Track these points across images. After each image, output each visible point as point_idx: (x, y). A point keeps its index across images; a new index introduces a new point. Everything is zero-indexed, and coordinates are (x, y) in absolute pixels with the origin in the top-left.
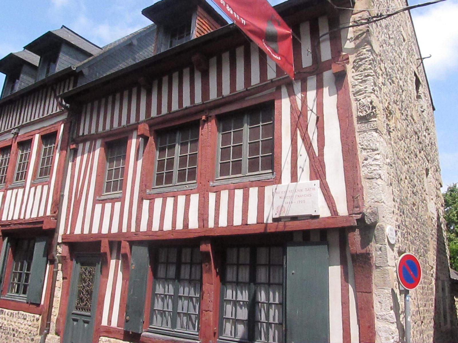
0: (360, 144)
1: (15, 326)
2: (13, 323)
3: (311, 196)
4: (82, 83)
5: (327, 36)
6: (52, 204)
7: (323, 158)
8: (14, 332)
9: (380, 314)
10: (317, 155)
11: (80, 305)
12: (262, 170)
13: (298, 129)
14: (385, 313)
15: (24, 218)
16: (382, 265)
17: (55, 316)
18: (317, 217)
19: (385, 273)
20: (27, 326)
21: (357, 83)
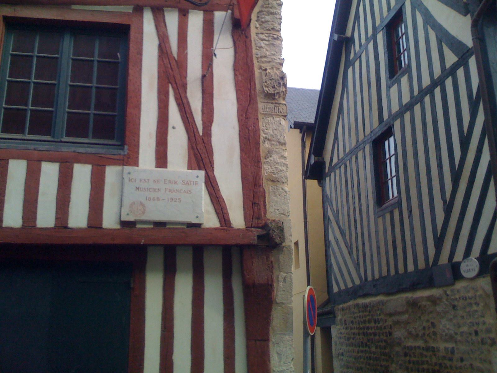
0: (263, 130)
3: (191, 193)
9: (279, 370)
10: (201, 134)
12: (30, 133)
14: (284, 368)
16: (284, 302)
18: (199, 225)
19: (288, 314)
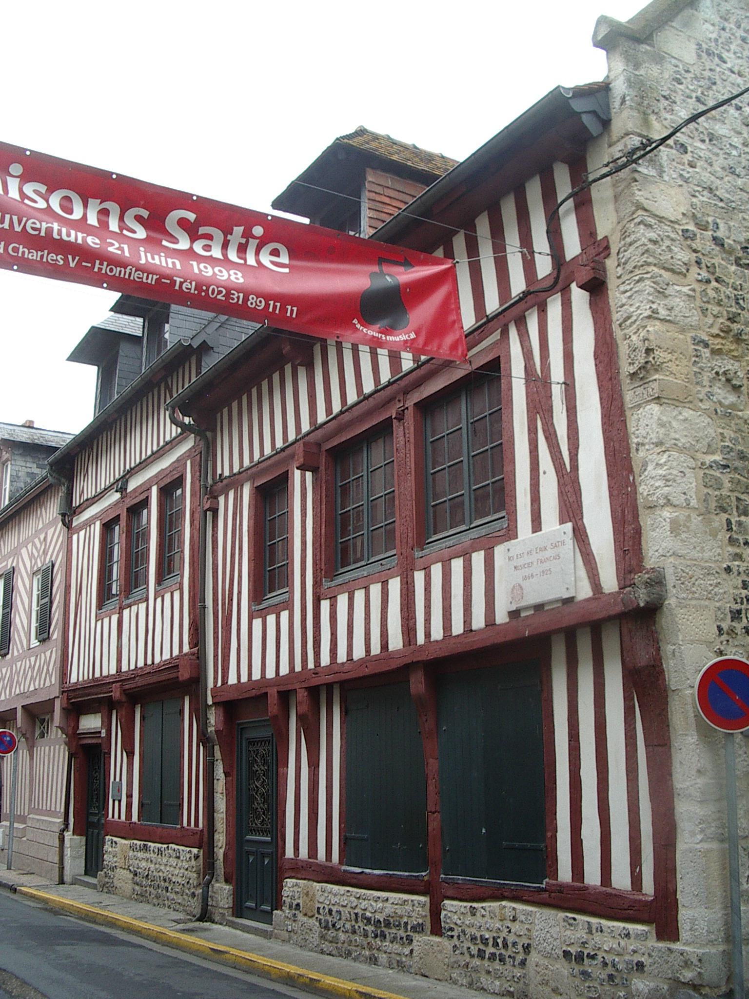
1: (166, 871)
2: (162, 868)
4: (210, 362)
5: (570, 203)
6: (190, 629)
7: (578, 474)
8: (167, 884)
10: (569, 470)
11: (256, 824)
13: (538, 416)
15: (153, 663)
16: (680, 687)
17: (221, 848)
20: (182, 871)
21: (624, 301)
